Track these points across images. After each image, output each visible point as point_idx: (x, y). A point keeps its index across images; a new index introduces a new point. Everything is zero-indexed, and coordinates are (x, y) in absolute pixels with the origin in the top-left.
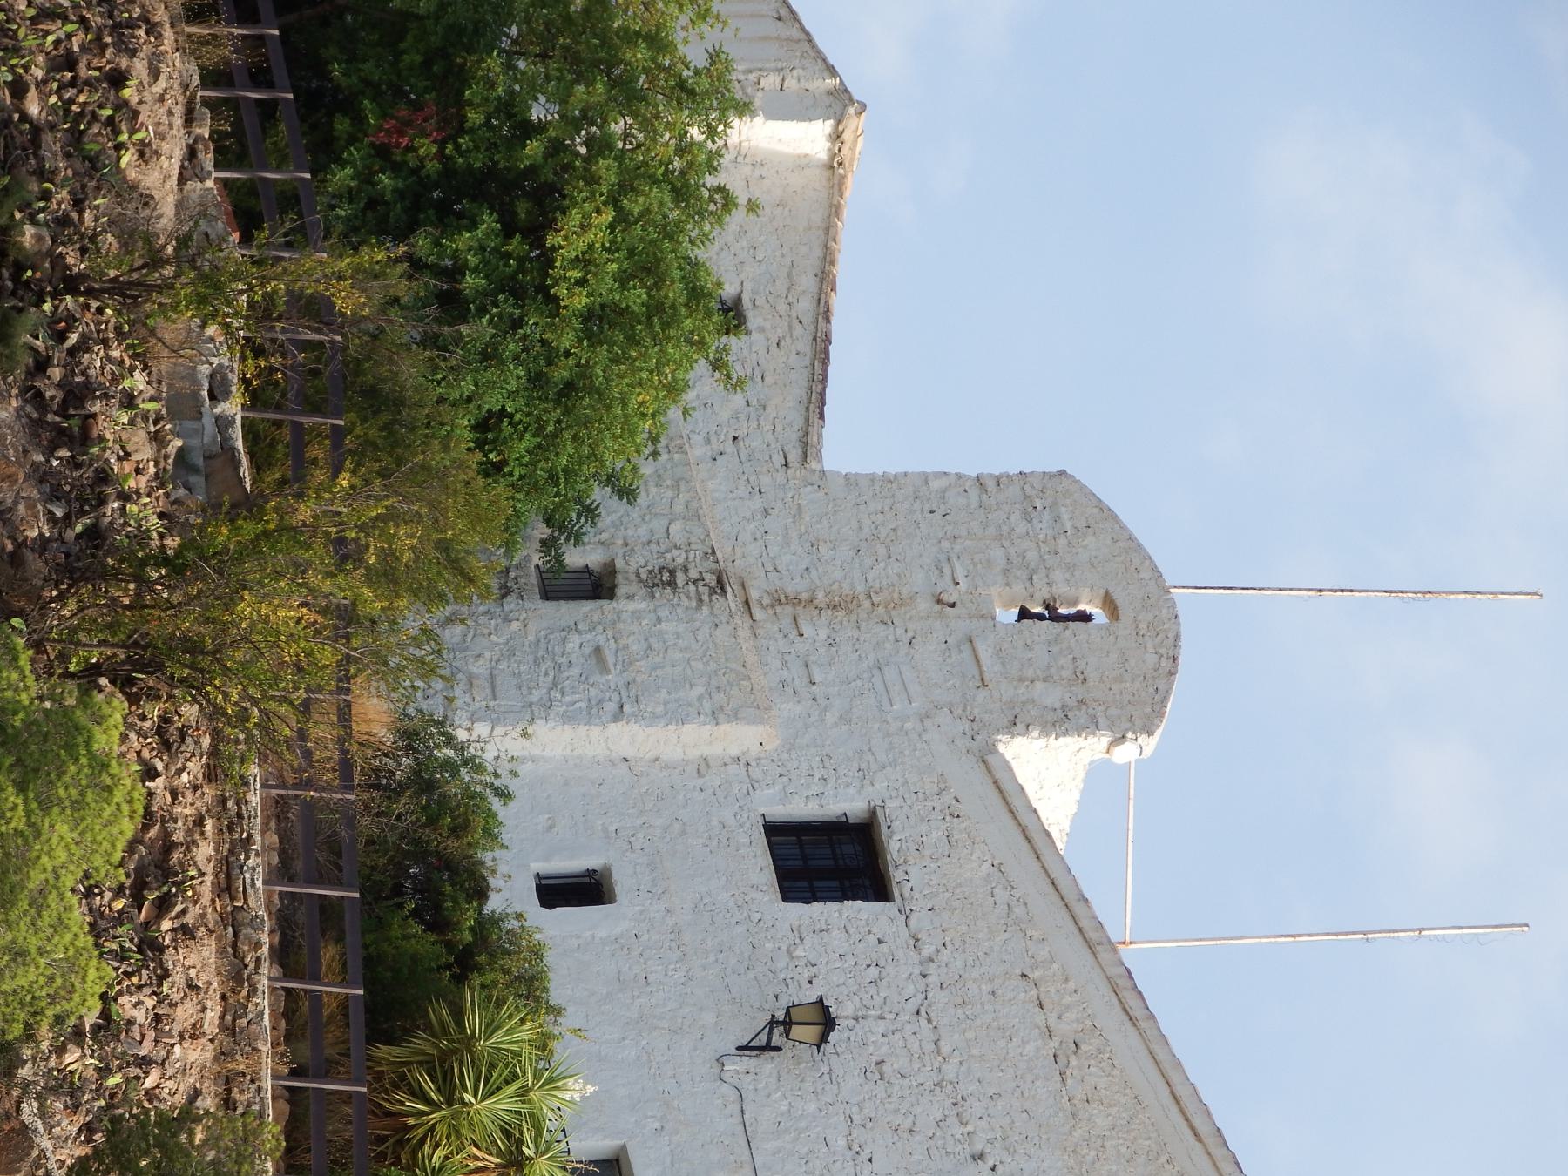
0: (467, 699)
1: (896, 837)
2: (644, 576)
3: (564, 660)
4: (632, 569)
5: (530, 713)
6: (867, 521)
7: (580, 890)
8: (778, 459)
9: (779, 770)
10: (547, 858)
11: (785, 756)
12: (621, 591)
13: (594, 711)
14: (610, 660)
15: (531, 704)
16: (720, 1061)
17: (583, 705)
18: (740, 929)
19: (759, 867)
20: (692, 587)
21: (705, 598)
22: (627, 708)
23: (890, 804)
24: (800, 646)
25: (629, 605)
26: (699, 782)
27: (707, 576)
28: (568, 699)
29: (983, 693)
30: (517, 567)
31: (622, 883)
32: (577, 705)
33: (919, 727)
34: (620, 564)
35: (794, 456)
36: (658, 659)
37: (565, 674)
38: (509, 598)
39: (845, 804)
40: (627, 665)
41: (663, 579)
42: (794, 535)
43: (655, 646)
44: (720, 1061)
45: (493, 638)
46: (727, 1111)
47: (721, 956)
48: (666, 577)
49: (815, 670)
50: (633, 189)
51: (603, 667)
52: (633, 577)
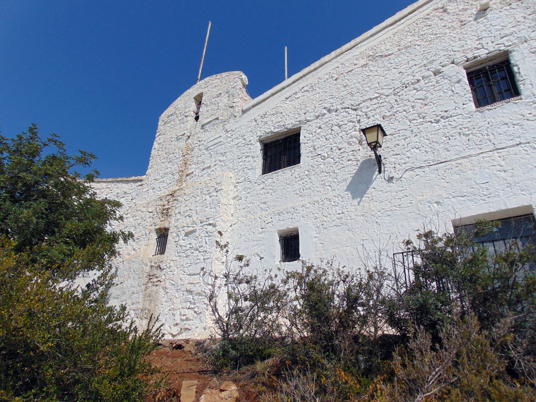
0: (198, 285)
1: (273, 130)
2: (163, 219)
3: (188, 246)
4: (160, 223)
5: (394, 335)
6: (162, 161)
7: (290, 245)
8: (141, 187)
9: (241, 172)
10: (301, 234)
11: (236, 171)
12: (167, 226)
13: (211, 234)
14: (191, 229)
15: (204, 259)
16: (390, 179)
17: (207, 238)
18: (313, 178)
19: (285, 174)
20: (170, 203)
21: (174, 198)
22: (211, 222)
23: (259, 134)
24: (197, 172)
25: (172, 223)
26: (243, 199)
27: (167, 198)
28: (204, 244)
29: (221, 118)
30: (151, 262)
31: (287, 225)
32: (207, 241)
33: (230, 132)
34: (157, 227)
35: (140, 183)
36: (193, 212)
37: (194, 245)
38: (161, 266)
39: (257, 150)
40: (194, 223)
41: (166, 213)
42: (162, 180)
43: (188, 213)
44: (390, 179)
45: (175, 273)
46: (422, 174)
47: (327, 184)
48: (165, 212)
49: (205, 166)
50: (435, 323)
51: (194, 231)
52: (163, 222)
